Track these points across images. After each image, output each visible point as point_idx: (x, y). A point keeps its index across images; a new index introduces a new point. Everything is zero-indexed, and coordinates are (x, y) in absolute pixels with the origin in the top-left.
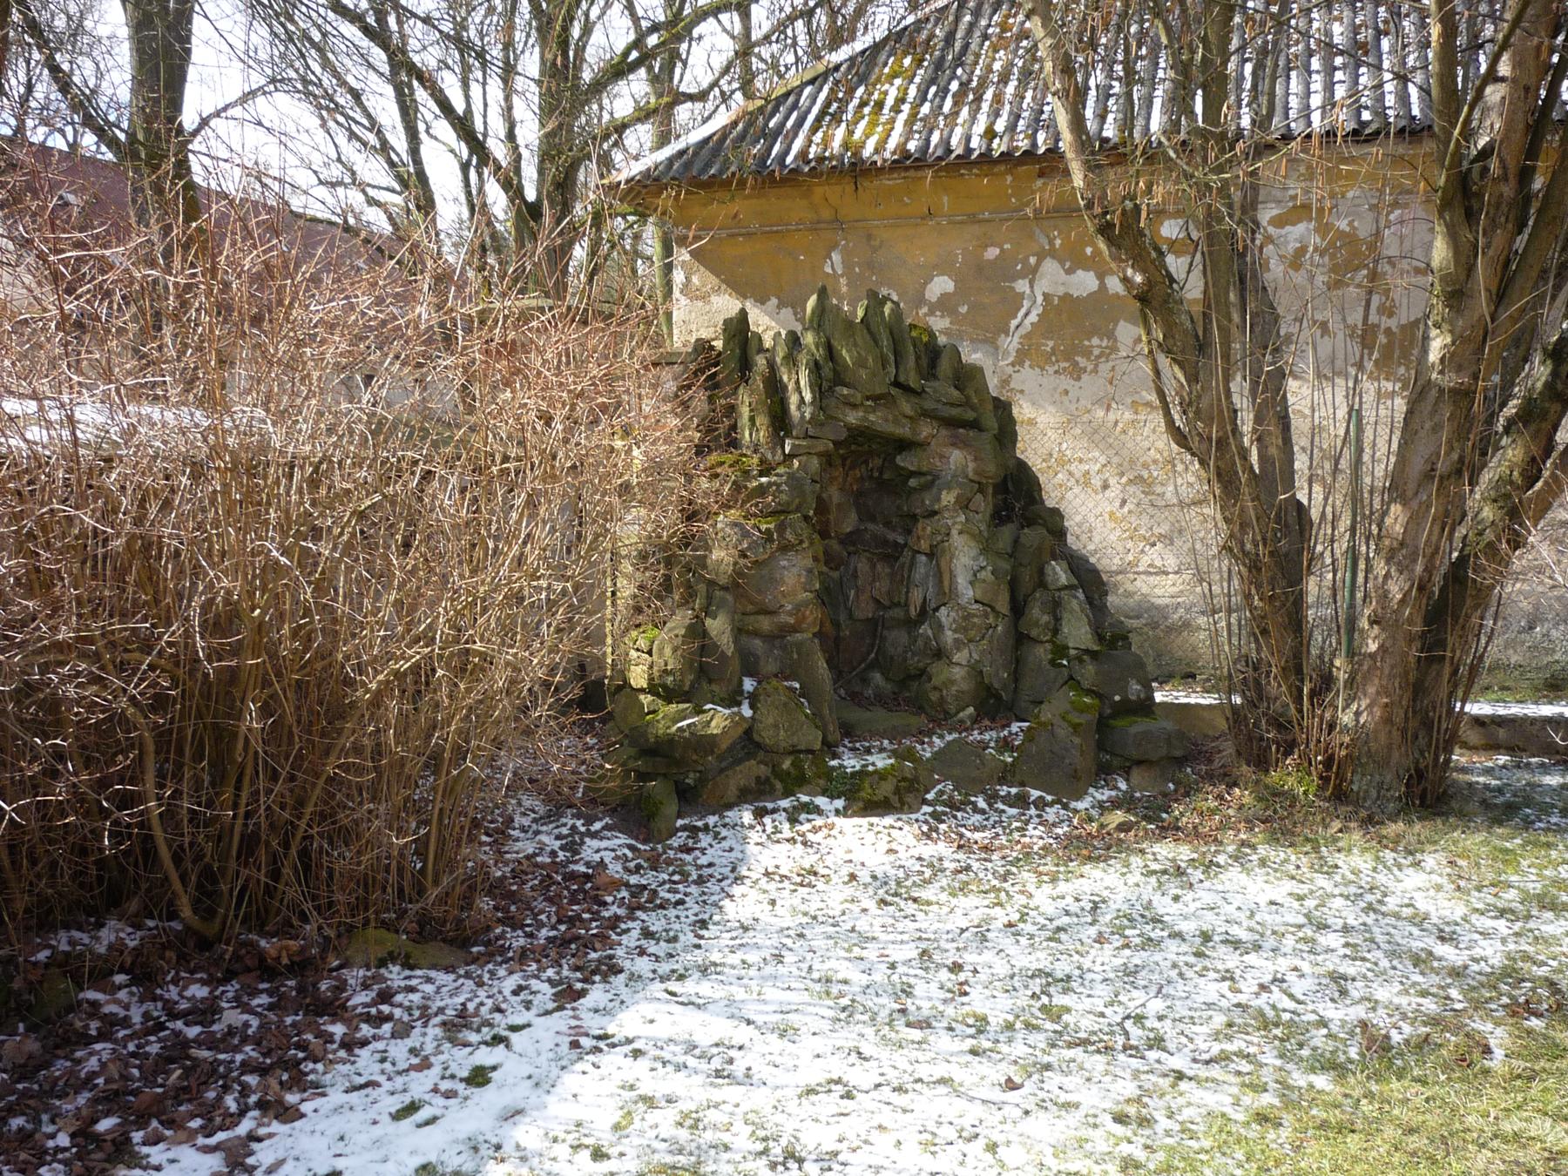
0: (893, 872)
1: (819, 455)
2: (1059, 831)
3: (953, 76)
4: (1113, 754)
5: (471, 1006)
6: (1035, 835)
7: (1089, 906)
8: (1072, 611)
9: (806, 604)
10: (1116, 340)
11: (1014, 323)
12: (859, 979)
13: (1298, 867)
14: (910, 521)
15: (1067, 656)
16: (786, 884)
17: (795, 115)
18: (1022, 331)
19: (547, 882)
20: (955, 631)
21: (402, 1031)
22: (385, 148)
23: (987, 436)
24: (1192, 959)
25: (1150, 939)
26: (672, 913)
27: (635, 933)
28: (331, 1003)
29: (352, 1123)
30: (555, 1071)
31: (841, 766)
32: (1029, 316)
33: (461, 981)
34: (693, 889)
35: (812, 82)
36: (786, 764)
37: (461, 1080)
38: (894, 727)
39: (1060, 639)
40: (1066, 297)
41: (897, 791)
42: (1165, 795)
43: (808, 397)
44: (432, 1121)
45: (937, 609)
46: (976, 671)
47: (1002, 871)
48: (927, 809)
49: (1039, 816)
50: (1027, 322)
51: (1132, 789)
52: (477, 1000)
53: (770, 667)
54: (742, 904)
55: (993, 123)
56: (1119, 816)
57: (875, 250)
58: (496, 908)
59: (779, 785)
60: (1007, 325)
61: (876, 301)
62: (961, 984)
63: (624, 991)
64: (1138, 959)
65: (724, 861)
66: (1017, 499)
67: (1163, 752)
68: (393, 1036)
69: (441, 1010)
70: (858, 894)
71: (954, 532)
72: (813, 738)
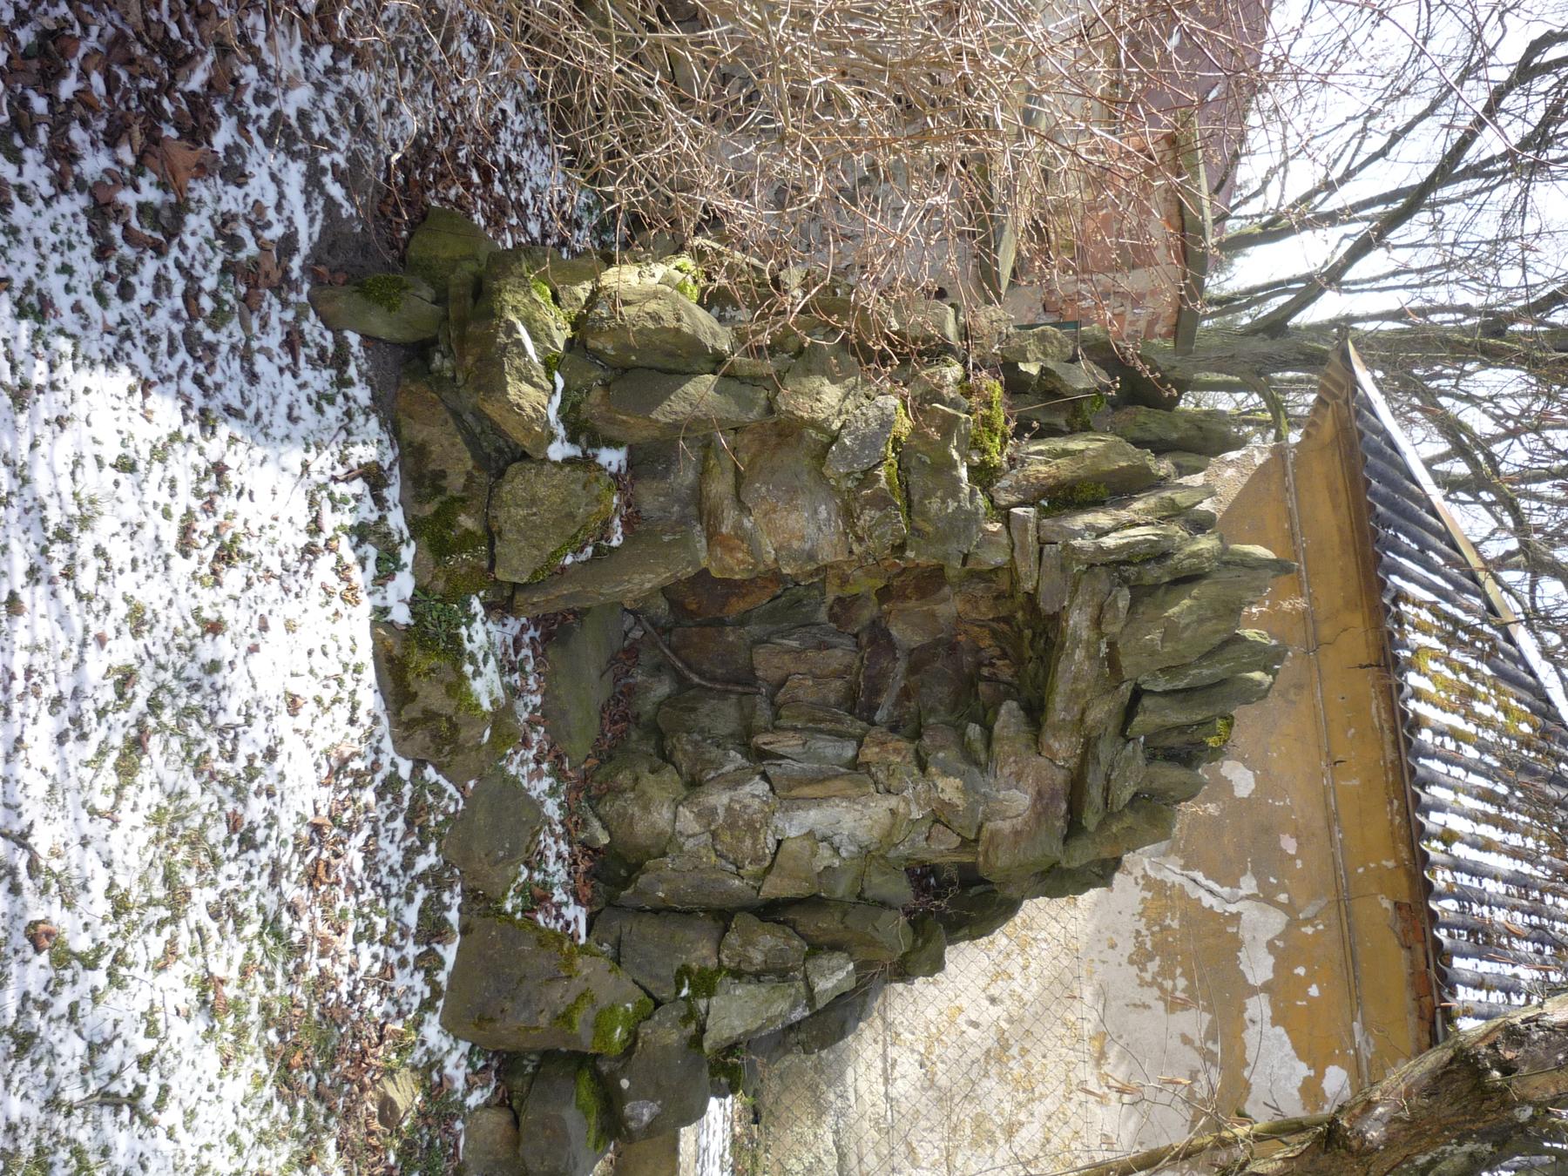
2: (372, 999)
6: (352, 961)
8: (769, 1002)
9: (755, 551)
11: (1199, 876)
14: (911, 728)
15: (696, 992)
16: (185, 499)
18: (1189, 887)
20: (729, 809)
22: (1329, 186)
23: (1056, 850)
31: (472, 618)
32: (1210, 896)
38: (563, 713)
39: (724, 981)
40: (1237, 943)
41: (429, 716)
43: (1110, 541)
45: (765, 777)
46: (665, 845)
47: (247, 906)
48: (405, 768)
49: (403, 963)
50: (1202, 893)
51: (470, 1115)
54: (108, 408)
55: (1462, 841)
56: (406, 1095)
59: (429, 509)
60: (1196, 867)
61: (1268, 659)
66: (958, 899)
71: (893, 802)
72: (515, 565)
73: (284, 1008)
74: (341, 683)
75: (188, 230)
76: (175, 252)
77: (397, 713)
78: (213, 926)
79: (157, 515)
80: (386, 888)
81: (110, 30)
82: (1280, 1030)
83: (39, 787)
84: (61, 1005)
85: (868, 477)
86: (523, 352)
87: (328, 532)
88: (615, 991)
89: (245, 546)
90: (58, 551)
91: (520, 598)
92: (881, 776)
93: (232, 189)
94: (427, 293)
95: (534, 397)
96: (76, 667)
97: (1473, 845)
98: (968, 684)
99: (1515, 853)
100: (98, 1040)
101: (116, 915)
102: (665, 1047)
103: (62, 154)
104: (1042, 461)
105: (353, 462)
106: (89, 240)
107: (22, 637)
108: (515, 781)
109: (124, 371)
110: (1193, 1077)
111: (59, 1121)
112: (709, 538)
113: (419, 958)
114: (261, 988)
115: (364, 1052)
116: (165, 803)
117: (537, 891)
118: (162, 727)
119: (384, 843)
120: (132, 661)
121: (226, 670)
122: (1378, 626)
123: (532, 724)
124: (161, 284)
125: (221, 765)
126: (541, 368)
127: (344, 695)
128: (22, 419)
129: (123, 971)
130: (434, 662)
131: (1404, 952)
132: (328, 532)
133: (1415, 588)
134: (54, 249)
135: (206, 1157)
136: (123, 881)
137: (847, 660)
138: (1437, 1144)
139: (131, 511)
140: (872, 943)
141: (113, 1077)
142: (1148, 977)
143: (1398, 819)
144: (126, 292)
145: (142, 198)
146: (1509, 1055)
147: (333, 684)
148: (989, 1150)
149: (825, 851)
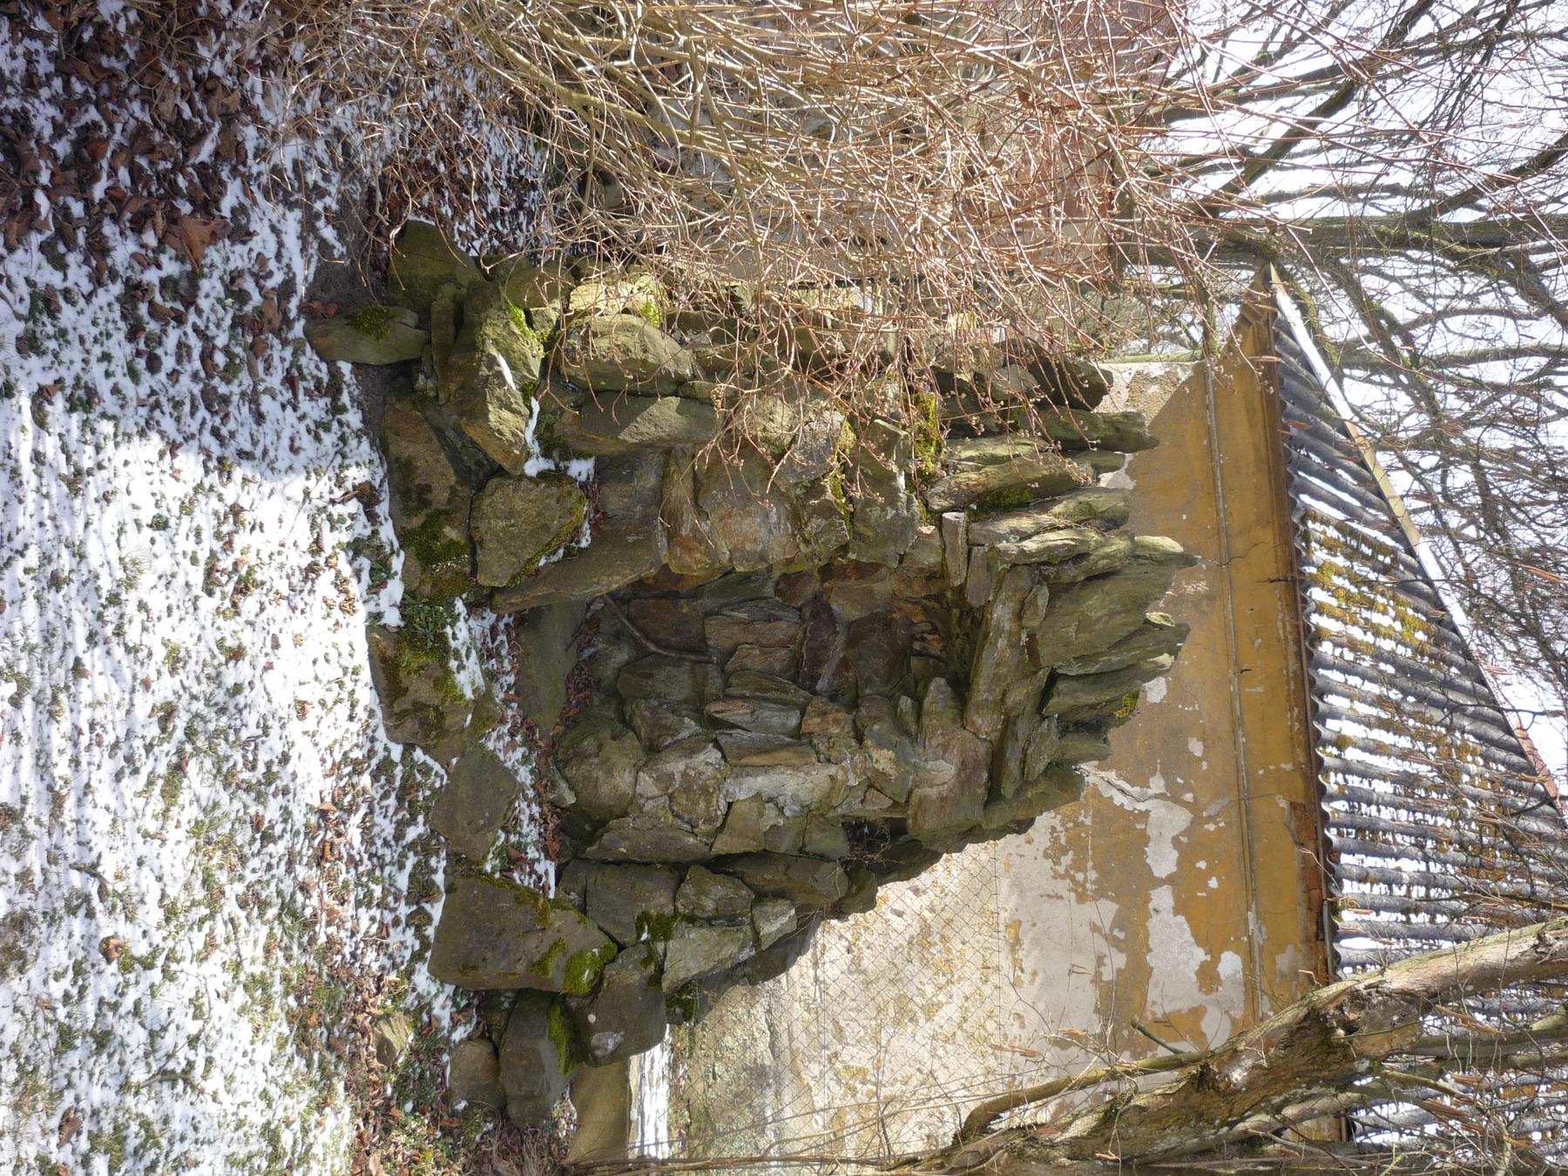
0: (252, 718)
1: (943, 564)
2: (371, 955)
3: (1405, 693)
4: (510, 1012)
8: (720, 945)
16: (209, 543)
17: (1356, 503)
18: (1102, 787)
20: (684, 775)
23: (977, 814)
27: (50, 277)
31: (456, 618)
35: (1394, 521)
36: (451, 533)
38: (535, 690)
39: (679, 926)
40: (1144, 839)
41: (419, 707)
42: (446, 1099)
43: (1030, 545)
45: (718, 746)
46: (626, 807)
47: (269, 892)
48: (396, 752)
54: (144, 472)
55: (1355, 745)
56: (402, 1036)
59: (417, 522)
66: (887, 847)
67: (512, 1090)
71: (833, 770)
72: (496, 570)
73: (302, 977)
74: (341, 684)
75: (202, 294)
76: (192, 317)
77: (390, 706)
78: (242, 914)
79: (186, 563)
80: (381, 858)
81: (132, 122)
82: (1181, 919)
83: (104, 821)
84: (128, 1003)
85: (815, 488)
86: (503, 382)
87: (328, 551)
88: (578, 936)
89: (259, 577)
90: (111, 614)
91: (498, 599)
92: (822, 748)
93: (239, 248)
94: (410, 318)
95: (512, 422)
96: (128, 712)
97: (1365, 749)
98: (902, 655)
99: (1404, 755)
100: (157, 1028)
101: (168, 920)
103: (98, 249)
104: (970, 463)
105: (348, 485)
106: (121, 324)
107: (86, 696)
108: (493, 755)
109: (155, 437)
110: (1100, 961)
111: (130, 1100)
112: (670, 539)
113: (411, 916)
114: (282, 961)
115: (365, 1002)
116: (201, 817)
117: (513, 853)
118: (197, 750)
119: (378, 819)
120: (171, 698)
121: (247, 691)
122: (1287, 543)
123: (507, 702)
124: (182, 350)
125: (246, 775)
126: (519, 394)
127: (345, 695)
128: (77, 503)
129: (174, 966)
130: (423, 660)
132: (328, 551)
133: (1323, 508)
134: (96, 341)
135: (242, 1112)
136: (173, 891)
137: (792, 631)
139: (164, 564)
140: (813, 891)
141: (169, 1056)
142: (1061, 870)
143: (1297, 726)
144: (154, 365)
145: (163, 274)
146: (1352, 1016)
147: (335, 687)
148: (910, 1027)
149: (771, 811)
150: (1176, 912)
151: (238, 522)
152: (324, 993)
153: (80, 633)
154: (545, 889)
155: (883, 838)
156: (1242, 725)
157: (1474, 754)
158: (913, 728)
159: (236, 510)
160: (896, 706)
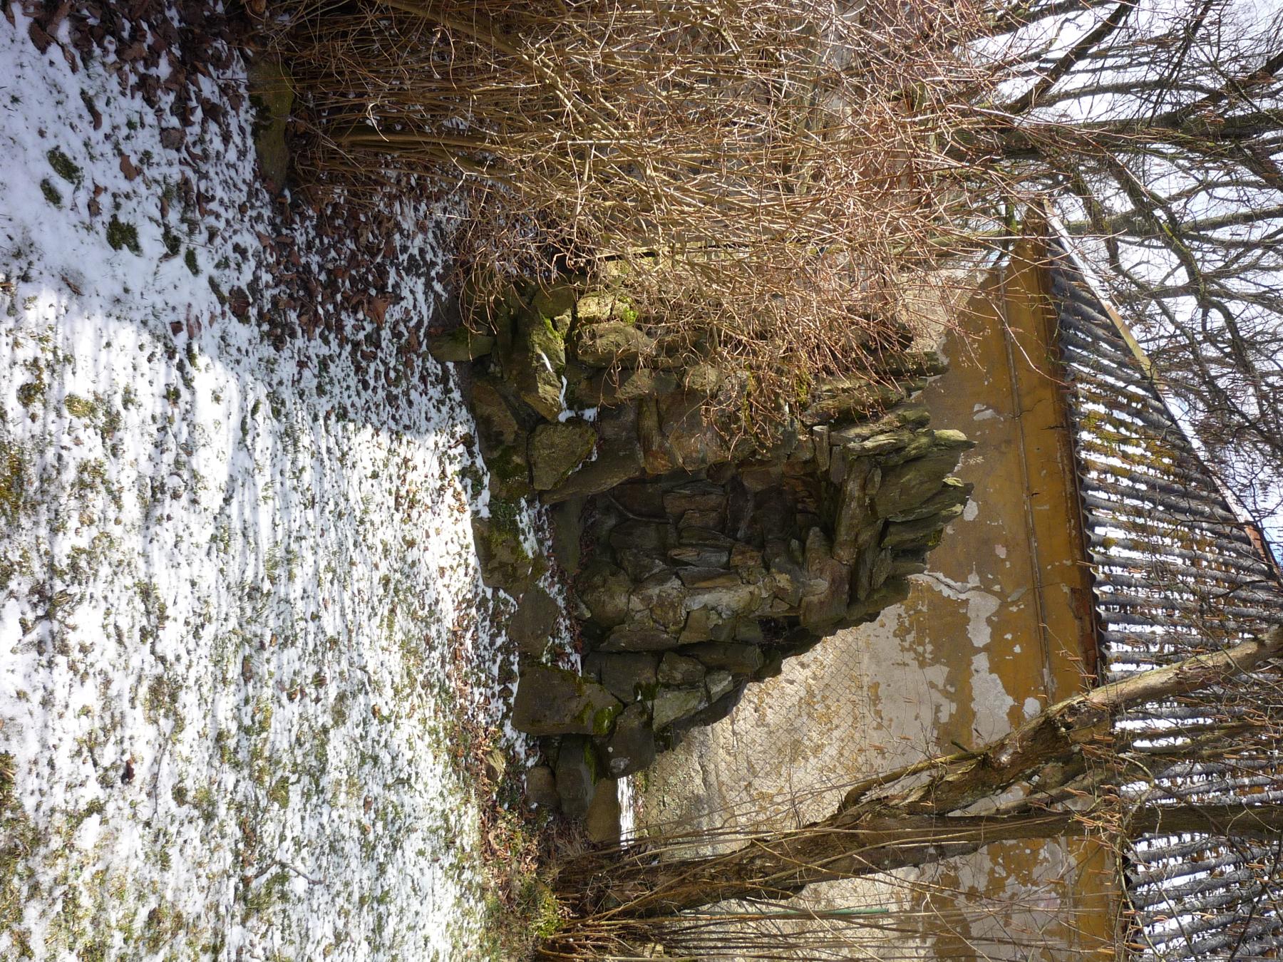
0: (421, 580)
2: (481, 717)
4: (559, 748)
5: (214, 206)
7: (404, 776)
9: (672, 459)
10: (931, 665)
11: (941, 576)
12: (295, 591)
13: (466, 946)
15: (645, 698)
16: (397, 482)
19: (372, 251)
20: (659, 596)
21: (169, 139)
24: (356, 897)
25: (374, 848)
26: (353, 381)
27: (325, 351)
28: (198, 58)
29: (39, 106)
30: (138, 316)
31: (521, 510)
33: (245, 188)
34: (381, 394)
36: (517, 459)
37: (114, 217)
40: (967, 620)
41: (502, 565)
42: (526, 802)
43: (869, 444)
44: (52, 195)
45: (678, 577)
46: (624, 617)
49: (493, 695)
50: (942, 587)
51: (528, 771)
52: (221, 210)
53: (609, 430)
54: (367, 446)
55: (1117, 545)
56: (500, 765)
57: (997, 448)
58: (336, 206)
59: (496, 454)
60: (939, 570)
62: (302, 691)
63: (253, 359)
64: (352, 848)
65: (415, 417)
66: (787, 635)
68: (163, 130)
69: (204, 176)
70: (394, 554)
71: (751, 588)
72: (545, 481)
73: (452, 728)
74: (460, 555)
79: (387, 495)
82: (995, 676)
89: (418, 497)
92: (745, 575)
95: (552, 392)
102: (631, 729)
119: (481, 634)
122: (1062, 399)
131: (1077, 622)
138: (1034, 764)
142: (907, 645)
149: (713, 616)
150: (991, 671)
151: (407, 467)
152: (462, 738)
153: (351, 541)
154: (576, 671)
155: (784, 628)
156: (1034, 533)
157: (1210, 545)
158: (800, 559)
159: (406, 461)
160: (789, 545)
